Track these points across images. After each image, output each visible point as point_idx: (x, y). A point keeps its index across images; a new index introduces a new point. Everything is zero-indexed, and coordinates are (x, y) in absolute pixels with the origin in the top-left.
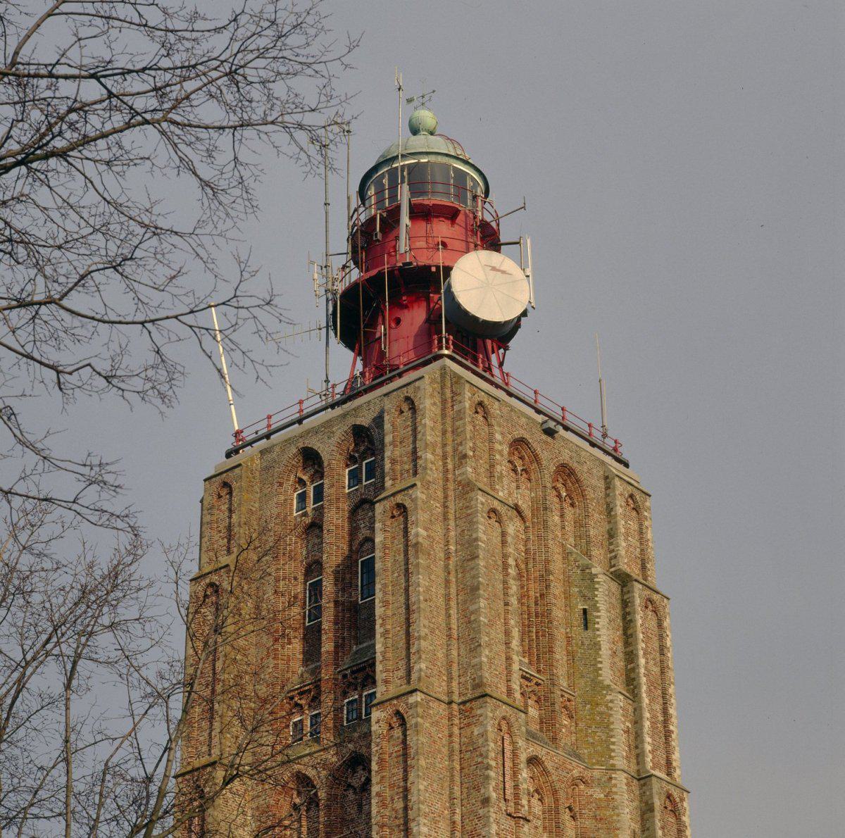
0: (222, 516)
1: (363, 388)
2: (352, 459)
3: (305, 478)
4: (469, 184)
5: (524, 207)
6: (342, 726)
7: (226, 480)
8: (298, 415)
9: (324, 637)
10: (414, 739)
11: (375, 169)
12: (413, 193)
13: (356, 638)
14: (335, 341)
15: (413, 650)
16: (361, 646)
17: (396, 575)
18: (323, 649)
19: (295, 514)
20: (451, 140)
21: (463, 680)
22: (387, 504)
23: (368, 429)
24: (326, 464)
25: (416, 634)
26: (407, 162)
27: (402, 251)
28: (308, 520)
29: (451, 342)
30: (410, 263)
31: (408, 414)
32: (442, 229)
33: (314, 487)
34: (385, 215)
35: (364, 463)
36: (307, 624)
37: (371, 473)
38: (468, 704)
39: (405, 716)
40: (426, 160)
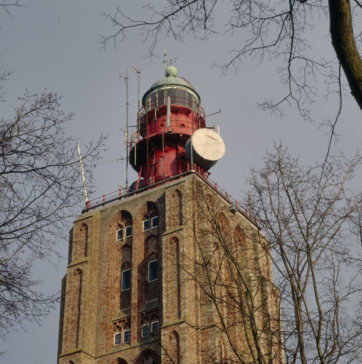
0: (82, 239)
1: (152, 185)
2: (146, 217)
3: (122, 224)
4: (194, 100)
5: (220, 112)
6: (141, 337)
7: (85, 223)
8: (119, 196)
9: (133, 296)
10: (183, 344)
11: (152, 89)
12: (172, 102)
13: (147, 298)
14: (130, 167)
15: (182, 303)
16: (150, 302)
17: (173, 269)
18: (132, 302)
19: (117, 240)
20: (187, 81)
21: (203, 318)
22: (168, 237)
23: (155, 203)
24: (134, 218)
25: (183, 296)
26: (167, 88)
27: (168, 126)
28: (124, 243)
29: (195, 167)
30: (171, 132)
31: (177, 197)
32: (182, 118)
33: (127, 229)
34: (158, 110)
35: (152, 219)
36: (122, 290)
37: (156, 223)
38: (206, 330)
39: (179, 333)
40: (176, 88)
